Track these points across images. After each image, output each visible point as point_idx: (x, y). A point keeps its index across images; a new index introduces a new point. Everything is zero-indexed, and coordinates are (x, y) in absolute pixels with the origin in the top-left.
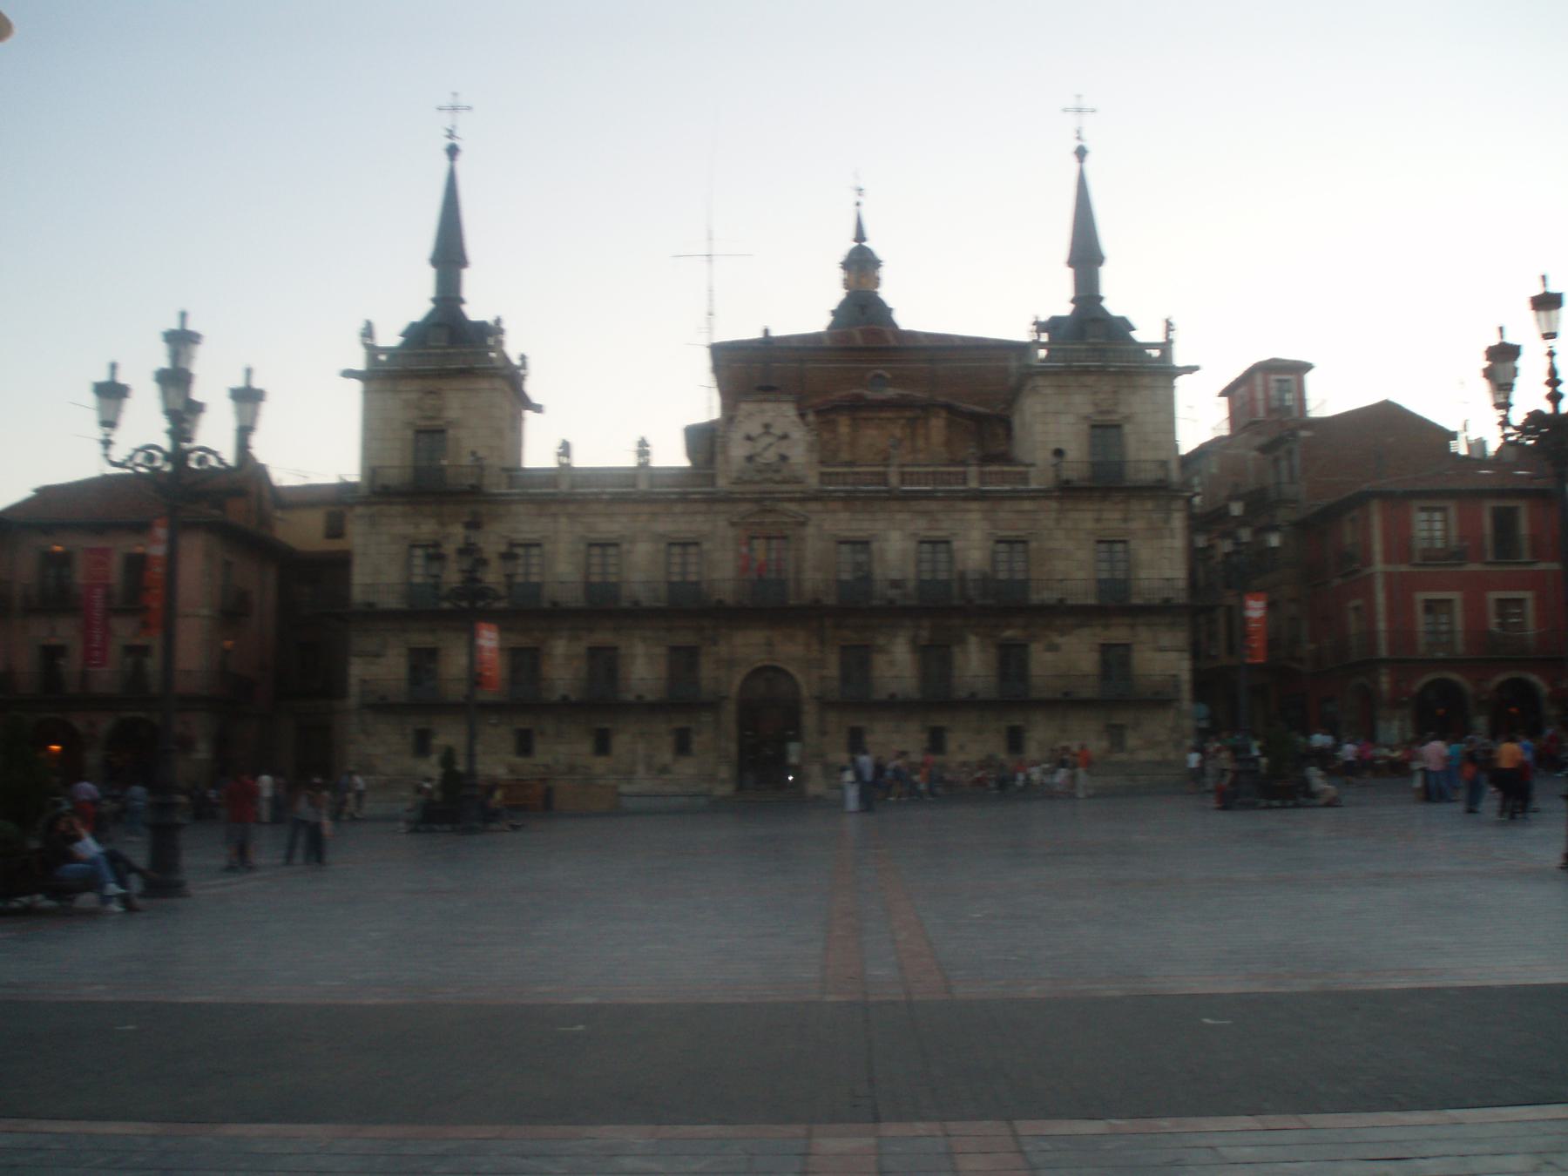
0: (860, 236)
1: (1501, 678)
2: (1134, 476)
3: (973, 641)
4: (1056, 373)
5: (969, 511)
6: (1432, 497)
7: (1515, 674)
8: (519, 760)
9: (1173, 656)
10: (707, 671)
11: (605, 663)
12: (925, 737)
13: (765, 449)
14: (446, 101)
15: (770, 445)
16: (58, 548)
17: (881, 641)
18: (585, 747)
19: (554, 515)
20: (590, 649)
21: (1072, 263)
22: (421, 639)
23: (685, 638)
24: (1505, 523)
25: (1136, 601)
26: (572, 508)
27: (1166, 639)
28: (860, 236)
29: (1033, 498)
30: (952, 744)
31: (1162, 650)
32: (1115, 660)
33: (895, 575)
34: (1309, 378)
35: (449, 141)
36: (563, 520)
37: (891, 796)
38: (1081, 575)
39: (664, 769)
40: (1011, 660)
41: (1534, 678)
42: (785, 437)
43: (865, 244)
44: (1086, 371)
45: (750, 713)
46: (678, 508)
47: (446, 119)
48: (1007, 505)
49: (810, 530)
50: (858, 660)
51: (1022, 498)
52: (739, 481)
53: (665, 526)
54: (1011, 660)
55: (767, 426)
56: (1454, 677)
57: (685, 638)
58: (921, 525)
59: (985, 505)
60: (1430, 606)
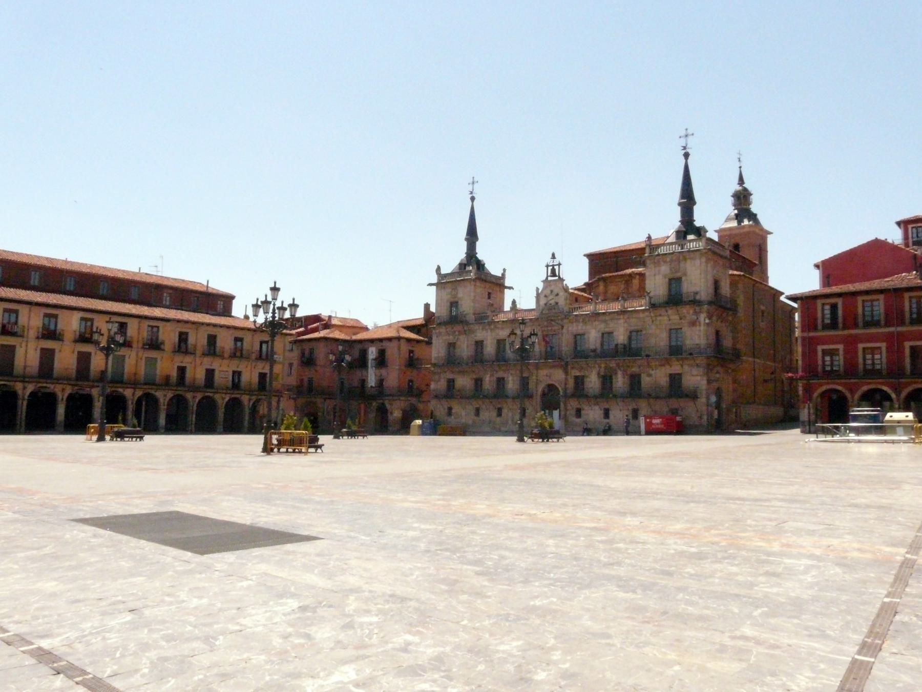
0: (741, 181)
8: (476, 418)
9: (699, 378)
12: (602, 412)
14: (476, 180)
28: (741, 181)
30: (612, 414)
33: (592, 347)
34: (234, 302)
35: (684, 151)
37: (345, 428)
38: (662, 344)
42: (557, 295)
49: (564, 331)
55: (552, 291)
60: (825, 352)
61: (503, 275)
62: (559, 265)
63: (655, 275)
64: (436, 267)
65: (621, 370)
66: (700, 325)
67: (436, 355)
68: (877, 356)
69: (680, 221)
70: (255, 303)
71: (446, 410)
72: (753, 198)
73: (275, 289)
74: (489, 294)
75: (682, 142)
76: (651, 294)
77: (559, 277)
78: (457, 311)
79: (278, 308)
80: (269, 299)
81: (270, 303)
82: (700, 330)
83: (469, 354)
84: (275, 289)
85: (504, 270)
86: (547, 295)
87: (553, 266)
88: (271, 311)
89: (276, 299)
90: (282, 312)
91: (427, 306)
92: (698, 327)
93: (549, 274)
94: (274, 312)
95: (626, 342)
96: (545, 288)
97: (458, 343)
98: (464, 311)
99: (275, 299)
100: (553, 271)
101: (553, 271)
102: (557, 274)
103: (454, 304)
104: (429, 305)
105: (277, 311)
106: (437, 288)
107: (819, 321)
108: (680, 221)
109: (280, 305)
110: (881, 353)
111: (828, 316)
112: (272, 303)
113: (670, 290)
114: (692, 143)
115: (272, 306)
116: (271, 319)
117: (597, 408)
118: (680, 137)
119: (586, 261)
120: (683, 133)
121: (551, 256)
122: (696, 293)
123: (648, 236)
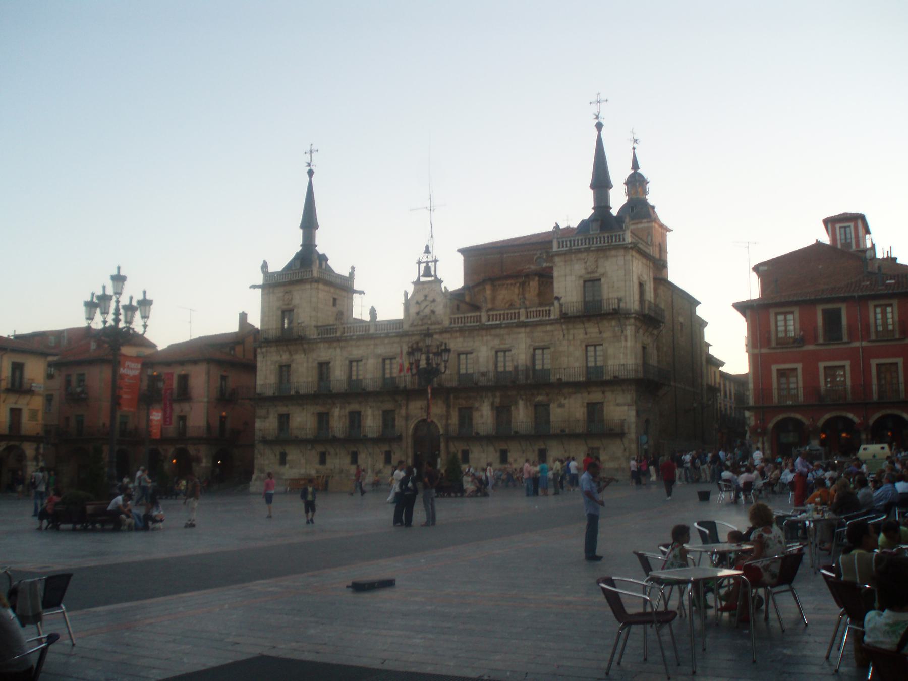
0: (635, 166)
1: (827, 416)
2: (606, 307)
3: (521, 403)
4: (565, 254)
5: (519, 333)
6: (883, 297)
7: (838, 413)
8: (321, 467)
10: (400, 423)
11: (355, 419)
12: (498, 454)
13: (424, 308)
14: (315, 148)
15: (427, 306)
16: (155, 373)
17: (477, 404)
18: (348, 460)
19: (335, 348)
20: (588, 404)
21: (302, 226)
22: (283, 410)
23: (389, 406)
24: (832, 319)
25: (606, 378)
26: (342, 344)
27: (621, 399)
28: (635, 166)
29: (551, 324)
31: (618, 405)
32: (594, 410)
33: (483, 369)
35: (597, 121)
36: (338, 350)
38: (577, 365)
39: (380, 472)
40: (541, 412)
41: (850, 415)
42: (434, 301)
43: (639, 171)
44: (579, 251)
45: (418, 441)
46: (386, 341)
47: (308, 156)
48: (539, 329)
50: (466, 416)
51: (547, 324)
52: (412, 325)
53: (381, 350)
54: (541, 412)
55: (426, 296)
56: (798, 416)
57: (389, 406)
58: (496, 342)
59: (528, 330)
60: (782, 373)
61: (352, 275)
62: (436, 261)
63: (566, 276)
64: (262, 263)
65: (522, 400)
66: (626, 340)
67: (262, 383)
68: (793, 380)
69: (593, 208)
70: (89, 299)
71: (278, 457)
72: (650, 187)
73: (118, 279)
74: (335, 300)
75: (594, 109)
76: (562, 300)
77: (436, 276)
78: (290, 323)
79: (125, 307)
80: (110, 291)
81: (110, 298)
82: (626, 347)
83: (310, 379)
84: (118, 279)
85: (353, 268)
86: (419, 301)
87: (427, 262)
88: (112, 310)
89: (120, 294)
90: (129, 313)
91: (243, 317)
92: (623, 343)
93: (421, 274)
94: (117, 313)
95: (529, 363)
96: (416, 292)
97: (293, 366)
98: (303, 322)
99: (118, 293)
100: (427, 269)
101: (427, 269)
102: (433, 273)
103: (287, 312)
104: (246, 315)
105: (122, 311)
106: (262, 291)
107: (872, 329)
108: (593, 208)
109: (127, 302)
110: (796, 377)
111: (792, 328)
112: (114, 299)
113: (585, 297)
114: (604, 110)
115: (113, 304)
116: (113, 323)
117: (491, 449)
118: (607, 101)
119: (460, 258)
120: (594, 98)
121: (424, 249)
122: (620, 300)
123: (555, 225)
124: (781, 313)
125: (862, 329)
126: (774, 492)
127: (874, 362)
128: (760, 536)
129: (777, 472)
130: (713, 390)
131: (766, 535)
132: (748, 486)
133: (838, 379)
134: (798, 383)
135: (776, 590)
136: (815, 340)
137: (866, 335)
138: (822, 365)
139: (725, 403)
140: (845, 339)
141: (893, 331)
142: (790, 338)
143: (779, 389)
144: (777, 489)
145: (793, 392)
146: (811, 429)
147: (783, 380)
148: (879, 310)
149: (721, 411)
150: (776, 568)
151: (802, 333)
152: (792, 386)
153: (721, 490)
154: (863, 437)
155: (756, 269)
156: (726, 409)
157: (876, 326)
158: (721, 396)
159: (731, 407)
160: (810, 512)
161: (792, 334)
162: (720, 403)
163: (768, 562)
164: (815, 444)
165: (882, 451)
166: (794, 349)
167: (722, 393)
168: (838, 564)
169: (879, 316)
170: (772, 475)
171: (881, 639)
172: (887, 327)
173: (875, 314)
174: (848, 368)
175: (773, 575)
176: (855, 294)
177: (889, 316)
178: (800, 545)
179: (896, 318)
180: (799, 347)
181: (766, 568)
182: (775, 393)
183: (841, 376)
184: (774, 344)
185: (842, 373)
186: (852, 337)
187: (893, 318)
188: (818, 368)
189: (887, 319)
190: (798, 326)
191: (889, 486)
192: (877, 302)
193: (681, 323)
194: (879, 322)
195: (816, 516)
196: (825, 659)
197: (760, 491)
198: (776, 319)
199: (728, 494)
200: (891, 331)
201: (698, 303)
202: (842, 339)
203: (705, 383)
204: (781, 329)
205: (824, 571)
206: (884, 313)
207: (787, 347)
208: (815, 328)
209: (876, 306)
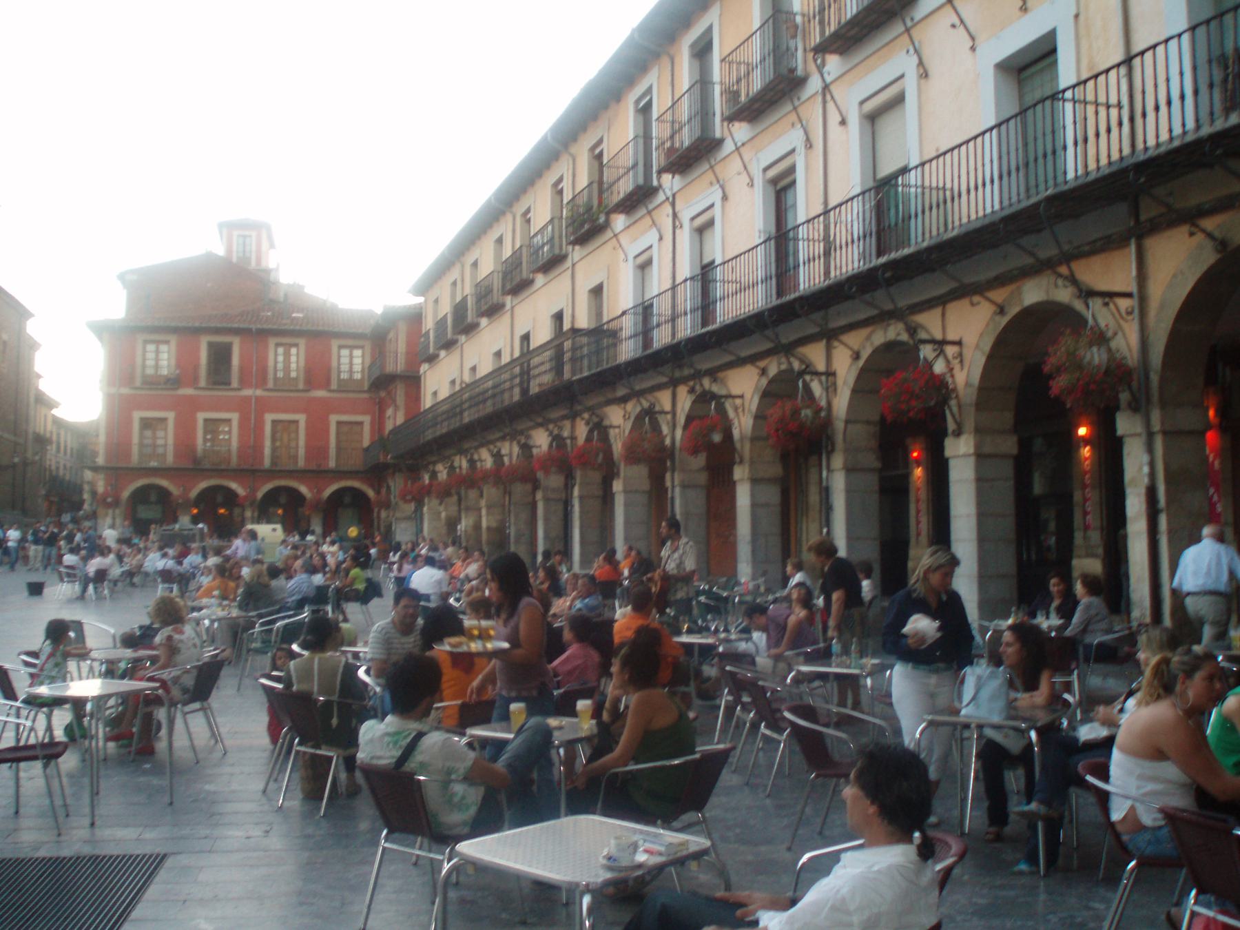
1: (203, 485)
24: (220, 357)
41: (234, 486)
56: (164, 483)
60: (147, 424)
68: (160, 434)
107: (271, 376)
110: (166, 430)
124: (152, 342)
125: (257, 374)
126: (133, 585)
127: (269, 418)
128: (169, 638)
129: (140, 556)
130: (42, 441)
131: (176, 636)
132: (101, 575)
133: (221, 437)
134: (167, 439)
135: (187, 709)
136: (194, 382)
137: (262, 381)
138: (201, 416)
139: (56, 460)
140: (235, 384)
141: (296, 379)
142: (160, 376)
143: (141, 445)
144: (136, 580)
145: (160, 450)
146: (180, 501)
147: (148, 433)
148: (281, 350)
149: (51, 471)
150: (189, 681)
151: (178, 372)
152: (160, 442)
153: (62, 580)
154: (248, 514)
155: (122, 277)
156: (58, 468)
157: (276, 370)
158: (52, 449)
159: (65, 466)
160: (214, 608)
161: (165, 372)
162: (50, 460)
163: (179, 673)
164: (184, 521)
165: (274, 534)
166: (165, 393)
167: (54, 446)
168: (288, 672)
169: (281, 358)
170: (130, 562)
171: (379, 753)
172: (289, 374)
173: (276, 355)
174: (235, 424)
175: (185, 691)
176: (253, 327)
177: (293, 359)
178: (214, 650)
179: (302, 363)
180: (172, 389)
181: (176, 680)
182: (135, 450)
183: (225, 432)
184: (138, 383)
185: (227, 429)
186: (244, 383)
187: (298, 362)
188: (195, 421)
189: (290, 363)
190: (173, 362)
191: (304, 576)
192: (343, 342)
193: (5, 343)
194: (280, 366)
195: (221, 613)
196: (260, 793)
197: (115, 582)
198: (144, 348)
199: (70, 585)
200: (294, 379)
201: (30, 315)
202: (230, 384)
203: (31, 431)
204: (150, 363)
205: (264, 681)
206: (287, 355)
207: (157, 389)
208: (196, 367)
209: (278, 345)
